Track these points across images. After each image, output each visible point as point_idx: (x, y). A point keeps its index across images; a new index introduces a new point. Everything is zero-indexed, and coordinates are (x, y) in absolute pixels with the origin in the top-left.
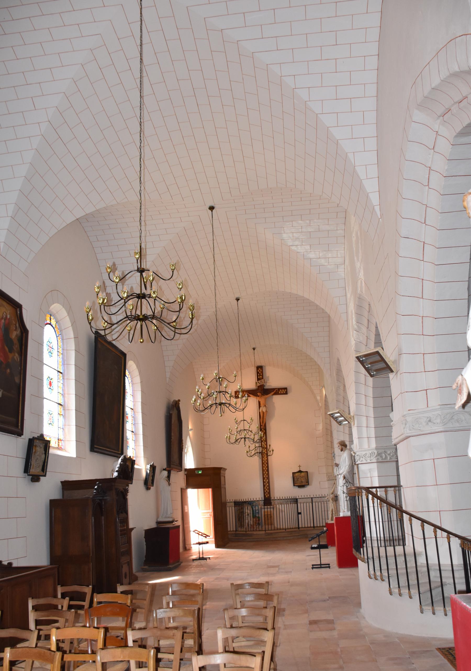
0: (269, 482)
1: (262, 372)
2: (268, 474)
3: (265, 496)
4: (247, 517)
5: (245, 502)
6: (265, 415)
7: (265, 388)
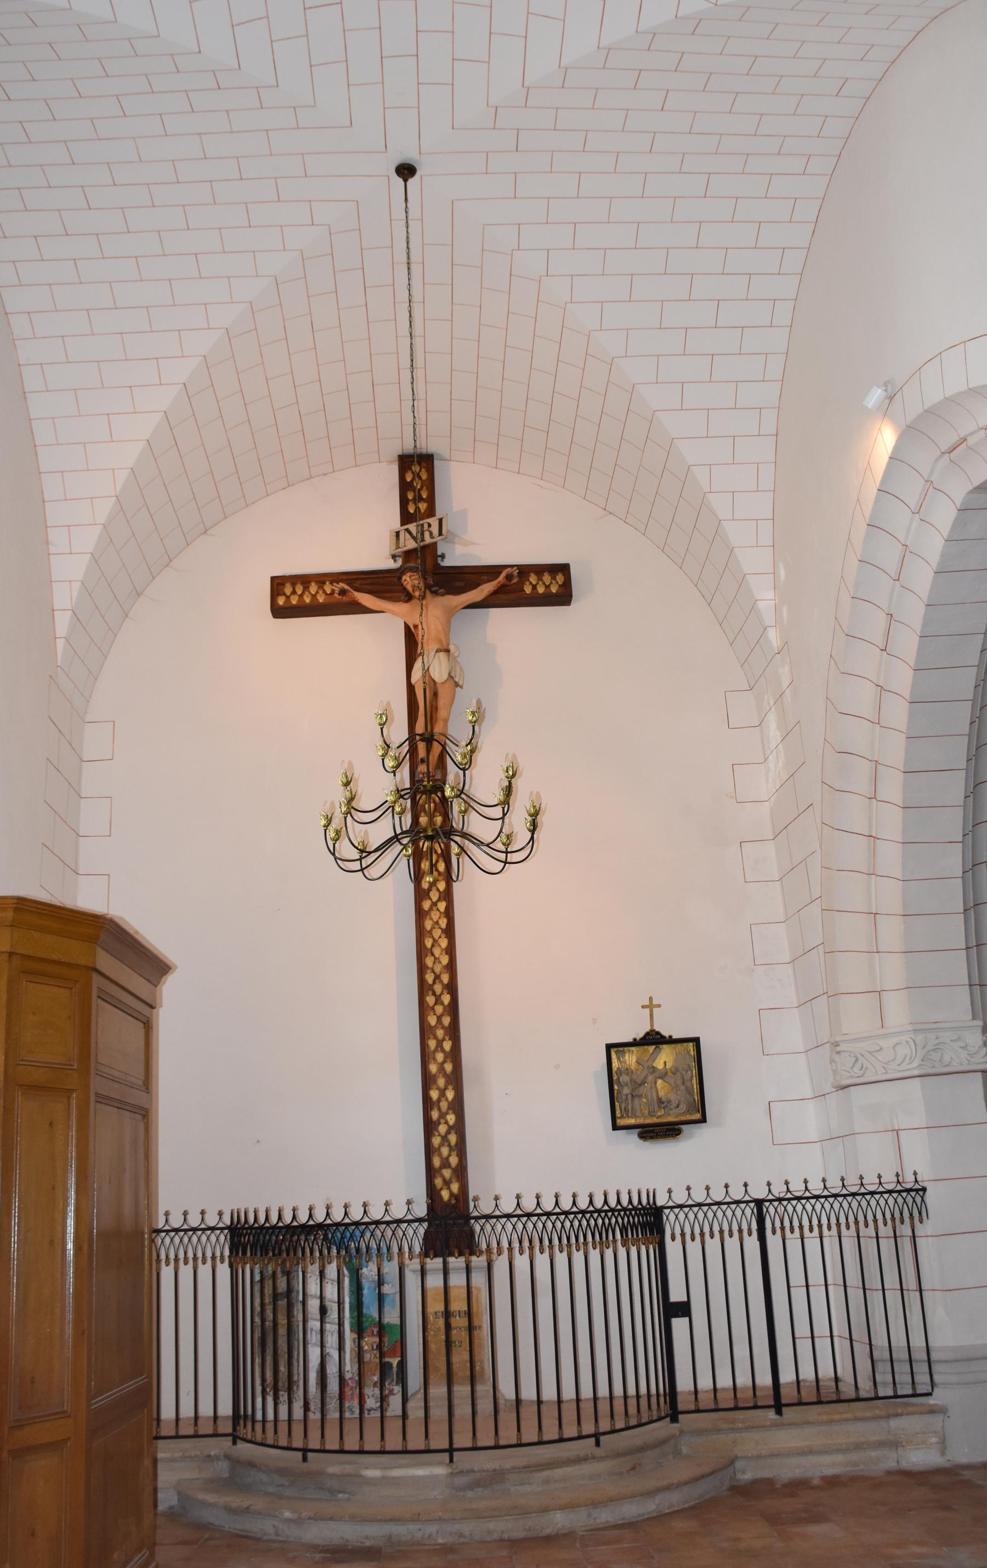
0: (458, 1106)
1: (430, 484)
2: (455, 1055)
3: (432, 1192)
4: (314, 1324)
5: (307, 1229)
6: (442, 702)
7: (447, 563)
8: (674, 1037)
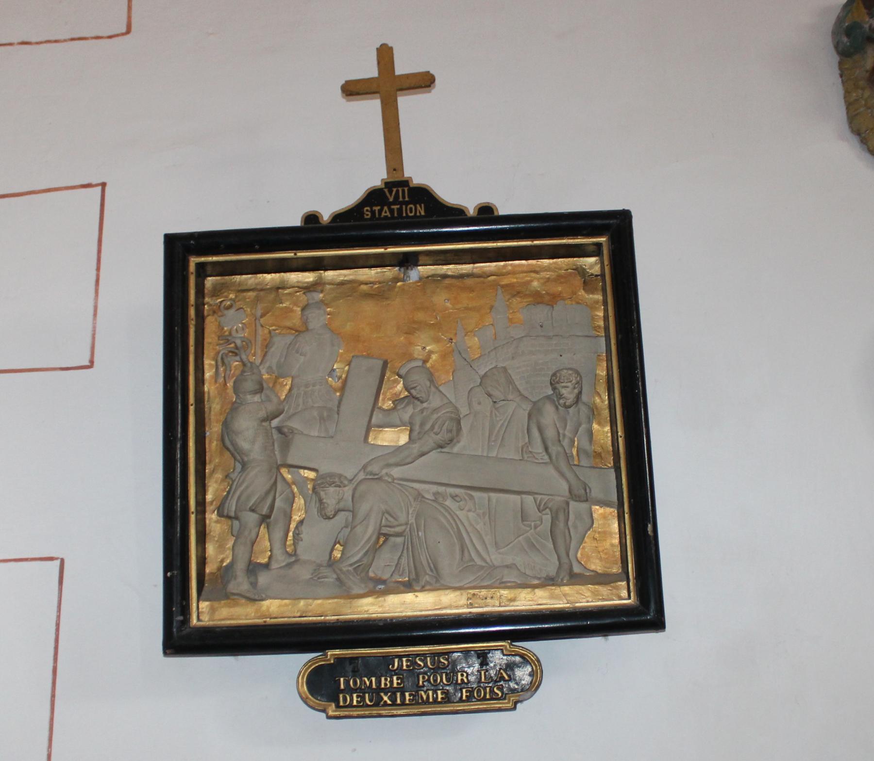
8: (503, 210)
